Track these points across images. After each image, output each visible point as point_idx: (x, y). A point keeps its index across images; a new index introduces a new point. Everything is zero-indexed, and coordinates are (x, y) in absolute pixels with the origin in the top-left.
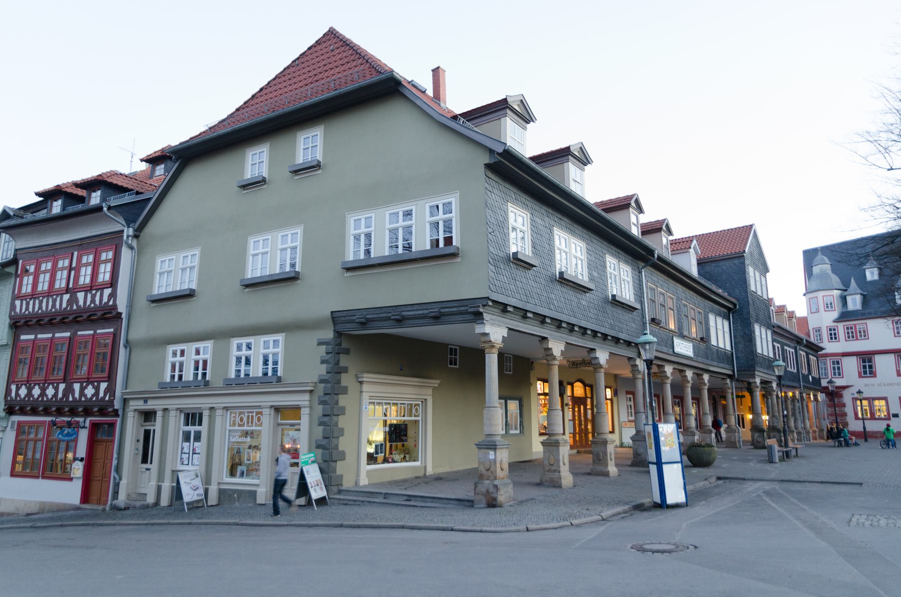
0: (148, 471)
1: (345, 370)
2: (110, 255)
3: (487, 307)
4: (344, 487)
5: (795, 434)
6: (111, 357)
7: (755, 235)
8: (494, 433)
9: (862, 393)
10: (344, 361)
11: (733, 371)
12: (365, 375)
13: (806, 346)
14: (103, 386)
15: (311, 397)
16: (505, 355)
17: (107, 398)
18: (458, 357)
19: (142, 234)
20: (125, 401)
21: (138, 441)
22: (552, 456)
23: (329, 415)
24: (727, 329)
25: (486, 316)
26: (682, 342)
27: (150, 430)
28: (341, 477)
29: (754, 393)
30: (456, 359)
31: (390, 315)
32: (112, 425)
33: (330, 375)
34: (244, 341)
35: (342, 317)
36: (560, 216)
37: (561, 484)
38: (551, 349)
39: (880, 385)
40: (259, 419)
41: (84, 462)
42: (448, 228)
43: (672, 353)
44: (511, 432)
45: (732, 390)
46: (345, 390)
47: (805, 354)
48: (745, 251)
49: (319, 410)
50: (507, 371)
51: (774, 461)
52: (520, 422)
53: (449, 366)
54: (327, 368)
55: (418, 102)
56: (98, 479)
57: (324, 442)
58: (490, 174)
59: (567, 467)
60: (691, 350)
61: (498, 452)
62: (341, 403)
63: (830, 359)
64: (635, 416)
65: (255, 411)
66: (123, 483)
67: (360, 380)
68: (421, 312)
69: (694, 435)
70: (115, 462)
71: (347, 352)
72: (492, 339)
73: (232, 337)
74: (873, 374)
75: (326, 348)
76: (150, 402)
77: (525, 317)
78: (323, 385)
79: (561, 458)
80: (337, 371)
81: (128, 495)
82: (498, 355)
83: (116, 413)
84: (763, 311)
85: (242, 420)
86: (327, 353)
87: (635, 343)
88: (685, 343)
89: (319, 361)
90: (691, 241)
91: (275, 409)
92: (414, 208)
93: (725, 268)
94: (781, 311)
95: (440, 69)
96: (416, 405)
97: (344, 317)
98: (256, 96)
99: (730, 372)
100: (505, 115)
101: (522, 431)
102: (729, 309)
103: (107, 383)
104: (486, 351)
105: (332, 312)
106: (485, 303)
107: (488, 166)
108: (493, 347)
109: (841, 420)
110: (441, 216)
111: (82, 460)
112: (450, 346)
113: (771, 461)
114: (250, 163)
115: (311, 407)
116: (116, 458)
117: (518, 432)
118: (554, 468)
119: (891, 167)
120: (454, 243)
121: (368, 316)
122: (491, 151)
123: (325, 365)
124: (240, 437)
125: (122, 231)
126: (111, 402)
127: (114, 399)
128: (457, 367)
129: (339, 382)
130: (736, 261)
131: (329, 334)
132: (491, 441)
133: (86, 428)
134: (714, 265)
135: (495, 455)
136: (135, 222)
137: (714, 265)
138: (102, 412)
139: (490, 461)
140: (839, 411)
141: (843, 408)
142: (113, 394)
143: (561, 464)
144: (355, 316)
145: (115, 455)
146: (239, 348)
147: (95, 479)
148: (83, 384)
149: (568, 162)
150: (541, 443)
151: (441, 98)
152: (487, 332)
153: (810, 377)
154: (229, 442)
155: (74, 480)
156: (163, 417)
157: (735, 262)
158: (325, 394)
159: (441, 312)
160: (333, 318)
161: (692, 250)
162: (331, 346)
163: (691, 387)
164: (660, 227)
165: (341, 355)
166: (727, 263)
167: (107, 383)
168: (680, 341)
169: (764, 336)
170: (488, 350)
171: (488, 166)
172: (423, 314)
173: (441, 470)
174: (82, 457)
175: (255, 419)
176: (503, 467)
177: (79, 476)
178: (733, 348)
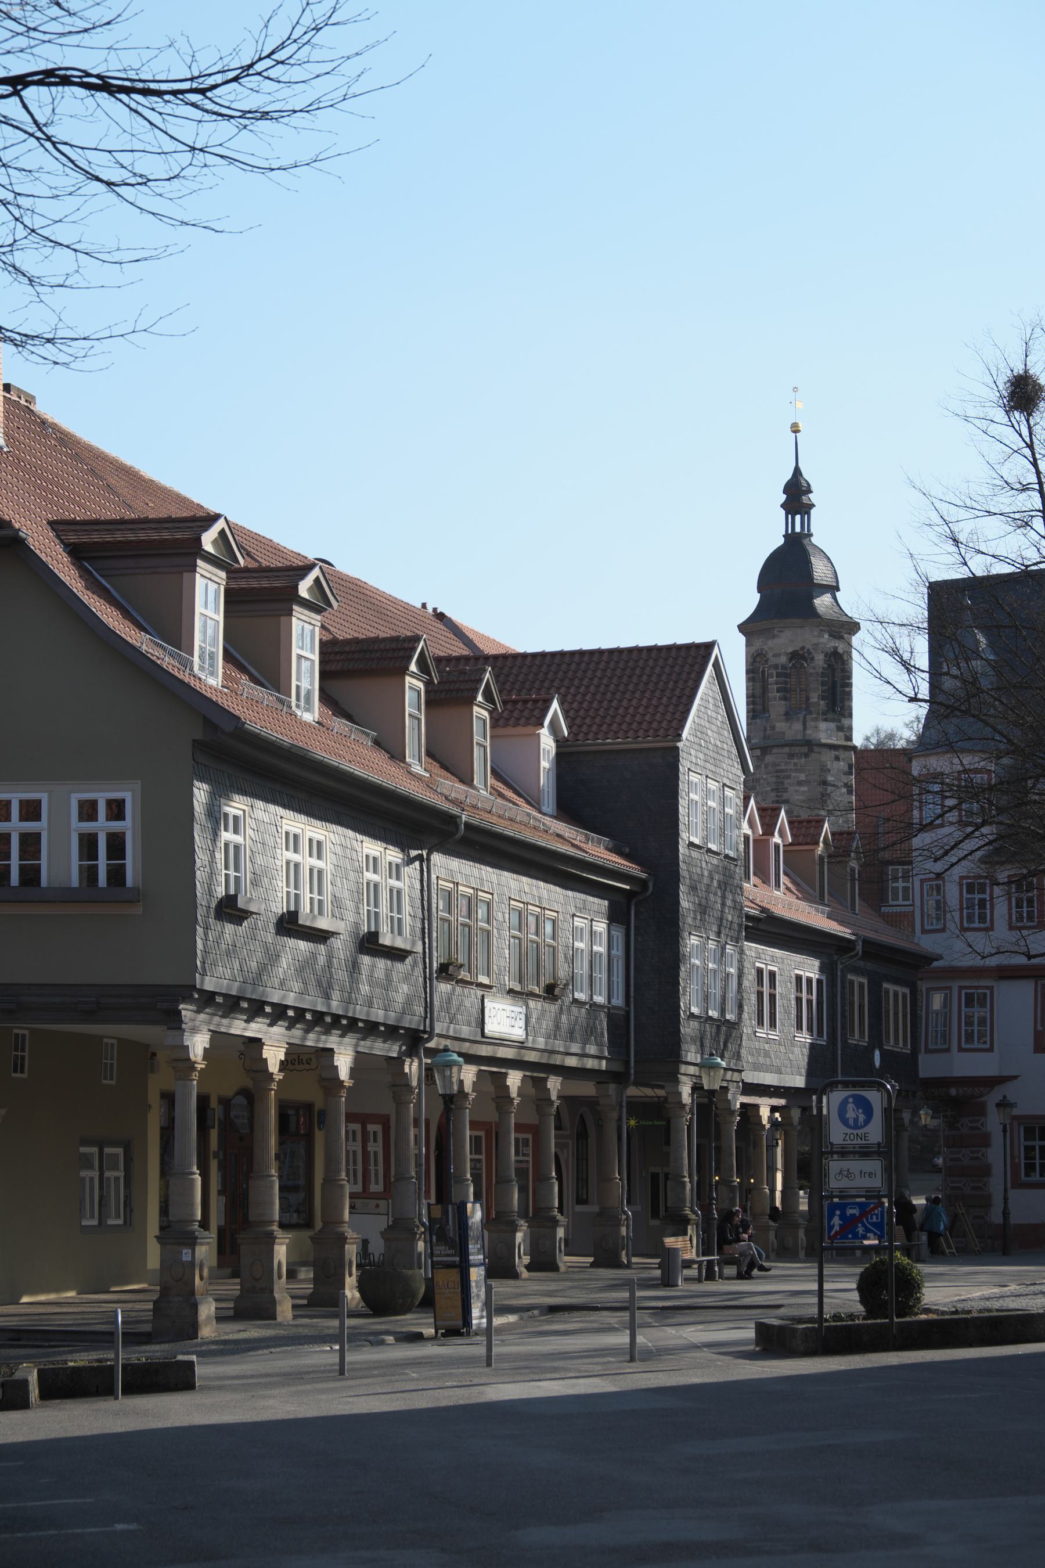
5: (801, 1234)
7: (717, 666)
11: (627, 1063)
16: (105, 1040)
42: (116, 845)
43: (479, 1038)
44: (110, 1222)
47: (865, 981)
50: (106, 1079)
52: (126, 1197)
63: (961, 988)
92: (44, 798)
101: (128, 1222)
109: (377, 1183)
110: (102, 826)
117: (120, 1222)
119: (916, 694)
120: (129, 882)
128: (25, 1076)
140: (972, 1159)
141: (984, 1150)
153: (877, 1053)
178: (632, 999)
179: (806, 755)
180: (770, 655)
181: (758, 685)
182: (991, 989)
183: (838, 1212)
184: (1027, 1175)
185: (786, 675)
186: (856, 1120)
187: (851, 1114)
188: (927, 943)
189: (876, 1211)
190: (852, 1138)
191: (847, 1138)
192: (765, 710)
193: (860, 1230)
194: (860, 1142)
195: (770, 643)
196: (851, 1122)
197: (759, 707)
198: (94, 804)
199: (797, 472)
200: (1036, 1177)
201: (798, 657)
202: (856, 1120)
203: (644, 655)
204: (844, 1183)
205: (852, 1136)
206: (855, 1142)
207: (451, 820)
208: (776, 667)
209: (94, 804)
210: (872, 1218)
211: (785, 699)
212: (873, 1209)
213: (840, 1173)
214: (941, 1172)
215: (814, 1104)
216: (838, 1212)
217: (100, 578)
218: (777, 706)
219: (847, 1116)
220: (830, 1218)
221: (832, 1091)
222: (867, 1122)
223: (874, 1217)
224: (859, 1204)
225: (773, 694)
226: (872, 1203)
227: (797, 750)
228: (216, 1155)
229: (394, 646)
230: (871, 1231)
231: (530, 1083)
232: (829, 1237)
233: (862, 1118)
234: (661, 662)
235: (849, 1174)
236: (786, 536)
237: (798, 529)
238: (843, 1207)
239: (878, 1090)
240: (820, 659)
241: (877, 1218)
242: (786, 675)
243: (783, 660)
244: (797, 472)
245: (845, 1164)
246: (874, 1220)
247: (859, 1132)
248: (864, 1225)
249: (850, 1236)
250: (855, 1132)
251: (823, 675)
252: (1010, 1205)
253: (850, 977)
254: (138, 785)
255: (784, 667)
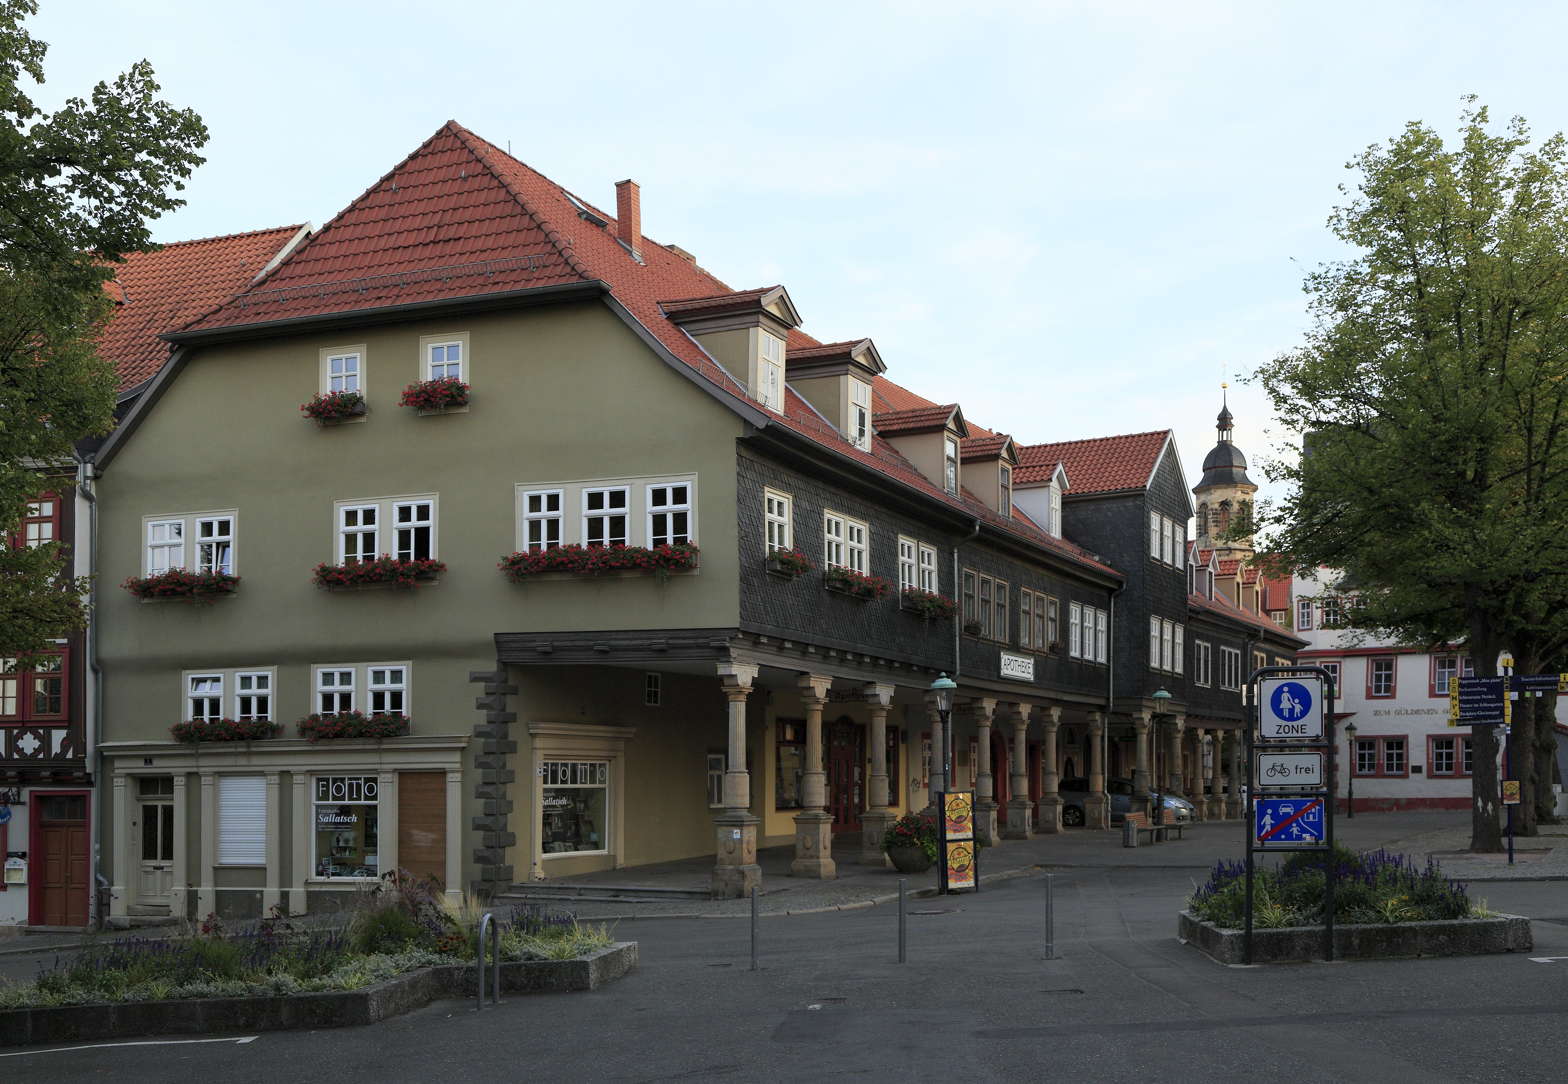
0: (158, 872)
1: (513, 718)
2: (48, 509)
3: (735, 641)
4: (516, 882)
5: (1223, 806)
6: (70, 685)
8: (740, 806)
9: (1355, 729)
10: (512, 704)
11: (1108, 699)
12: (541, 725)
13: (1266, 640)
14: (58, 736)
15: (462, 757)
17: (70, 755)
18: (659, 690)
19: (106, 474)
20: (104, 759)
21: (134, 824)
22: (808, 837)
23: (493, 783)
24: (1102, 626)
25: (734, 652)
26: (1014, 658)
27: (157, 806)
28: (511, 868)
29: (1138, 736)
30: (656, 693)
31: (592, 643)
32: (82, 800)
33: (493, 725)
34: (337, 670)
35: (512, 642)
36: (833, 490)
37: (820, 874)
38: (814, 688)
39: (1398, 713)
40: (371, 789)
41: (27, 859)
45: (1103, 731)
46: (512, 748)
47: (1264, 656)
48: (1145, 486)
49: (478, 775)
51: (1130, 844)
53: (648, 704)
54: (488, 715)
55: (636, 328)
56: (58, 885)
57: (488, 821)
58: (745, 453)
59: (828, 852)
60: (1031, 670)
61: (745, 831)
62: (509, 767)
64: (930, 779)
65: (363, 776)
66: (118, 888)
67: (532, 731)
68: (639, 642)
69: (1025, 808)
70: (94, 858)
71: (514, 691)
72: (740, 682)
73: (314, 663)
74: (1390, 692)
75: (485, 687)
76: (156, 763)
77: (781, 649)
78: (482, 740)
79: (821, 838)
80: (504, 720)
81: (128, 908)
82: (747, 703)
83: (88, 781)
84: (1171, 591)
85: (339, 790)
86: (486, 693)
87: (935, 669)
88: (1020, 659)
89: (474, 704)
90: (1054, 465)
91: (400, 773)
93: (1110, 514)
94: (1231, 572)
95: (632, 185)
96: (601, 765)
97: (517, 642)
98: (319, 241)
99: (1102, 702)
100: (757, 324)
102: (1111, 591)
103: (66, 731)
104: (730, 698)
105: (495, 634)
106: (733, 636)
107: (741, 441)
108: (741, 692)
111: (23, 856)
112: (649, 673)
113: (1126, 845)
114: (329, 373)
115: (463, 772)
116: (96, 852)
118: (809, 853)
121: (556, 644)
122: (746, 423)
123: (485, 712)
124: (337, 815)
125: (76, 469)
126: (79, 762)
127: (85, 757)
128: (658, 705)
129: (505, 736)
130: (1130, 503)
131: (490, 666)
132: (736, 817)
133: (23, 804)
134: (1093, 507)
135: (741, 833)
136: (96, 451)
137: (1093, 507)
138: (58, 778)
139: (734, 840)
142: (81, 748)
143: (821, 847)
144: (534, 641)
145: (94, 846)
146: (328, 678)
147: (50, 885)
148: (11, 733)
149: (847, 374)
150: (794, 819)
151: (633, 240)
152: (734, 673)
154: (317, 824)
155: (9, 889)
156: (188, 786)
157: (1127, 504)
158: (486, 753)
159: (668, 644)
160: (497, 642)
161: (1054, 483)
162: (494, 684)
163: (1026, 731)
164: (996, 452)
165: (507, 696)
166: (1115, 506)
167: (66, 731)
168: (1011, 658)
169: (1167, 636)
170: (733, 696)
171: (741, 441)
172: (641, 645)
173: (635, 862)
174: (24, 851)
175: (364, 790)
176: (750, 849)
177: (22, 882)
179: (1228, 555)
180: (1209, 504)
181: (1203, 520)
182: (1340, 662)
183: (1269, 811)
184: (1360, 770)
185: (1216, 514)
186: (1291, 711)
187: (1285, 705)
188: (1303, 636)
189: (1313, 810)
190: (1287, 730)
191: (1281, 730)
192: (1206, 532)
193: (1295, 830)
194: (1295, 734)
195: (1209, 497)
196: (1286, 713)
197: (1203, 531)
198: (663, 491)
199: (1225, 407)
200: (1365, 771)
201: (1225, 504)
202: (1291, 711)
203: (1123, 440)
204: (1279, 779)
205: (1287, 728)
206: (1290, 735)
207: (970, 522)
208: (1212, 510)
209: (663, 491)
210: (1308, 818)
211: (1217, 526)
212: (1310, 807)
213: (1273, 768)
214: (1413, 767)
215: (1244, 693)
216: (1269, 811)
217: (691, 338)
218: (1213, 531)
219: (1281, 707)
220: (1261, 818)
221: (1264, 680)
222: (1304, 713)
223: (1311, 816)
224: (1294, 803)
225: (1211, 523)
226: (1309, 801)
227: (1223, 552)
228: (248, 746)
229: (937, 412)
230: (1307, 832)
231: (1038, 709)
232: (1259, 838)
233: (1298, 708)
234: (1134, 444)
235: (1283, 770)
236: (1218, 442)
237: (1225, 439)
238: (1275, 806)
239: (1317, 678)
240: (1236, 507)
241: (1314, 818)
242: (1216, 514)
243: (1216, 506)
244: (1225, 407)
245: (1279, 759)
246: (1311, 819)
247: (1295, 724)
248: (1299, 825)
249: (1283, 837)
250: (1290, 724)
251: (1238, 513)
252: (1353, 788)
253: (1256, 653)
254: (695, 478)
255: (1216, 510)
